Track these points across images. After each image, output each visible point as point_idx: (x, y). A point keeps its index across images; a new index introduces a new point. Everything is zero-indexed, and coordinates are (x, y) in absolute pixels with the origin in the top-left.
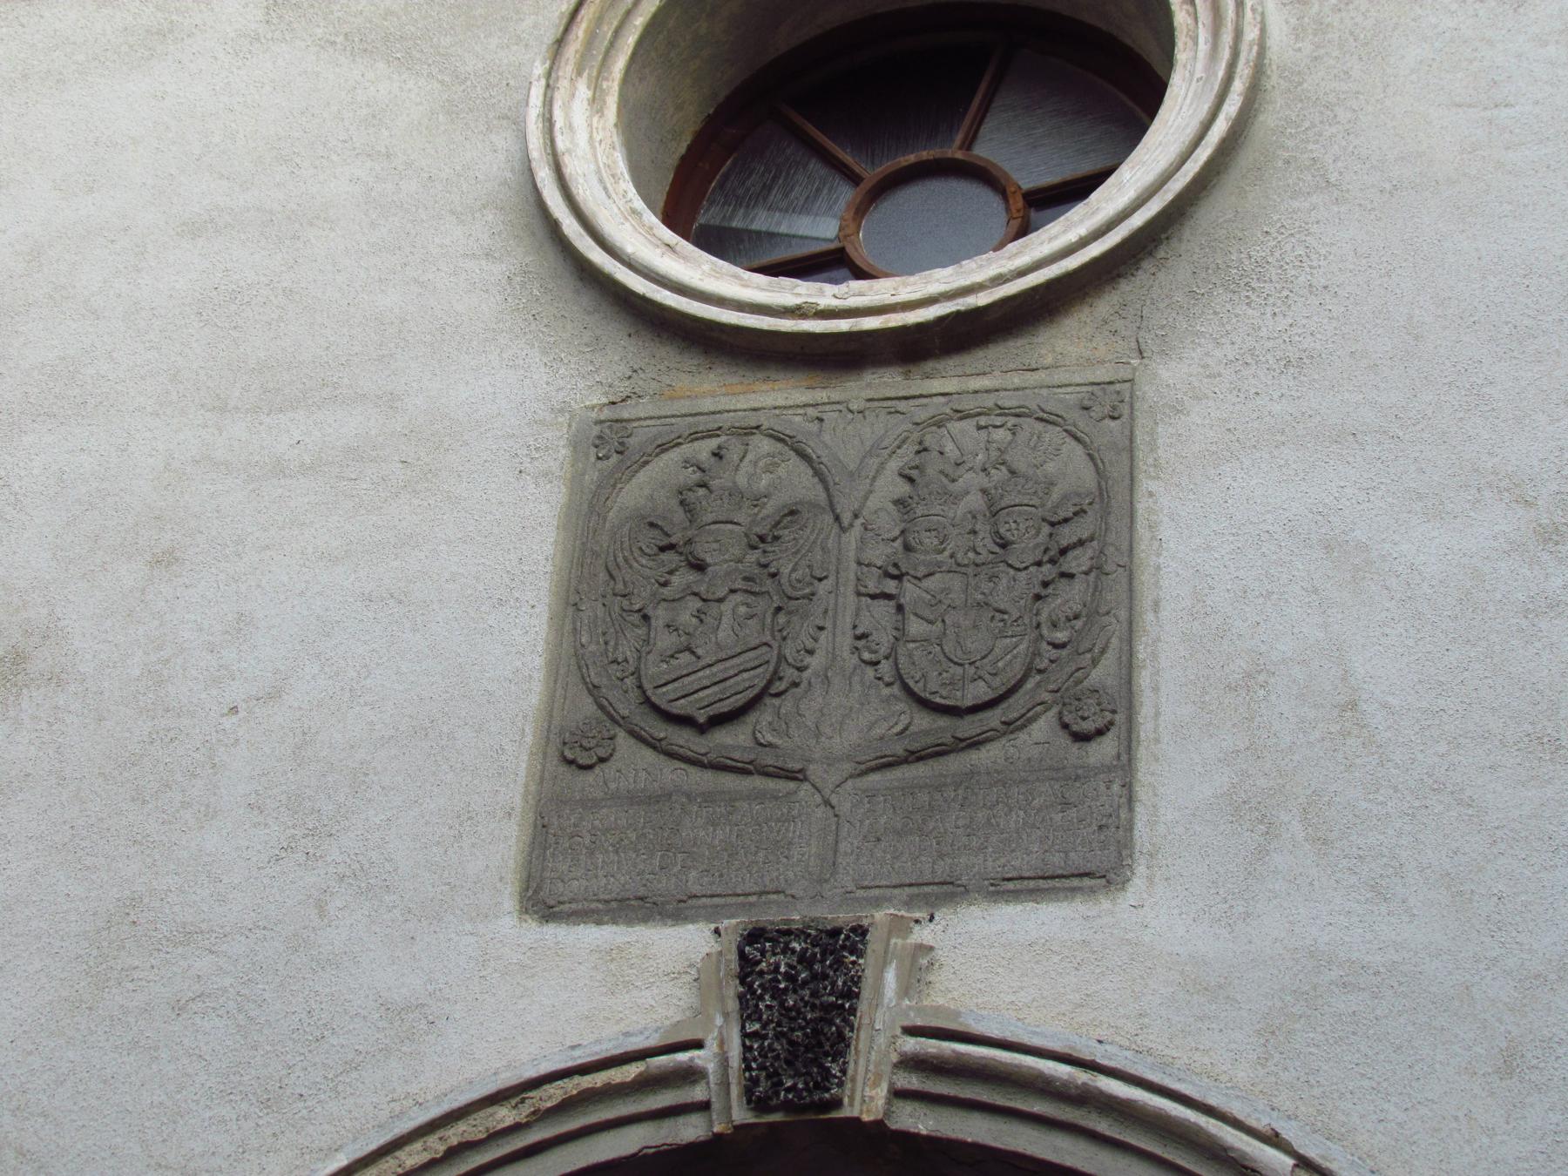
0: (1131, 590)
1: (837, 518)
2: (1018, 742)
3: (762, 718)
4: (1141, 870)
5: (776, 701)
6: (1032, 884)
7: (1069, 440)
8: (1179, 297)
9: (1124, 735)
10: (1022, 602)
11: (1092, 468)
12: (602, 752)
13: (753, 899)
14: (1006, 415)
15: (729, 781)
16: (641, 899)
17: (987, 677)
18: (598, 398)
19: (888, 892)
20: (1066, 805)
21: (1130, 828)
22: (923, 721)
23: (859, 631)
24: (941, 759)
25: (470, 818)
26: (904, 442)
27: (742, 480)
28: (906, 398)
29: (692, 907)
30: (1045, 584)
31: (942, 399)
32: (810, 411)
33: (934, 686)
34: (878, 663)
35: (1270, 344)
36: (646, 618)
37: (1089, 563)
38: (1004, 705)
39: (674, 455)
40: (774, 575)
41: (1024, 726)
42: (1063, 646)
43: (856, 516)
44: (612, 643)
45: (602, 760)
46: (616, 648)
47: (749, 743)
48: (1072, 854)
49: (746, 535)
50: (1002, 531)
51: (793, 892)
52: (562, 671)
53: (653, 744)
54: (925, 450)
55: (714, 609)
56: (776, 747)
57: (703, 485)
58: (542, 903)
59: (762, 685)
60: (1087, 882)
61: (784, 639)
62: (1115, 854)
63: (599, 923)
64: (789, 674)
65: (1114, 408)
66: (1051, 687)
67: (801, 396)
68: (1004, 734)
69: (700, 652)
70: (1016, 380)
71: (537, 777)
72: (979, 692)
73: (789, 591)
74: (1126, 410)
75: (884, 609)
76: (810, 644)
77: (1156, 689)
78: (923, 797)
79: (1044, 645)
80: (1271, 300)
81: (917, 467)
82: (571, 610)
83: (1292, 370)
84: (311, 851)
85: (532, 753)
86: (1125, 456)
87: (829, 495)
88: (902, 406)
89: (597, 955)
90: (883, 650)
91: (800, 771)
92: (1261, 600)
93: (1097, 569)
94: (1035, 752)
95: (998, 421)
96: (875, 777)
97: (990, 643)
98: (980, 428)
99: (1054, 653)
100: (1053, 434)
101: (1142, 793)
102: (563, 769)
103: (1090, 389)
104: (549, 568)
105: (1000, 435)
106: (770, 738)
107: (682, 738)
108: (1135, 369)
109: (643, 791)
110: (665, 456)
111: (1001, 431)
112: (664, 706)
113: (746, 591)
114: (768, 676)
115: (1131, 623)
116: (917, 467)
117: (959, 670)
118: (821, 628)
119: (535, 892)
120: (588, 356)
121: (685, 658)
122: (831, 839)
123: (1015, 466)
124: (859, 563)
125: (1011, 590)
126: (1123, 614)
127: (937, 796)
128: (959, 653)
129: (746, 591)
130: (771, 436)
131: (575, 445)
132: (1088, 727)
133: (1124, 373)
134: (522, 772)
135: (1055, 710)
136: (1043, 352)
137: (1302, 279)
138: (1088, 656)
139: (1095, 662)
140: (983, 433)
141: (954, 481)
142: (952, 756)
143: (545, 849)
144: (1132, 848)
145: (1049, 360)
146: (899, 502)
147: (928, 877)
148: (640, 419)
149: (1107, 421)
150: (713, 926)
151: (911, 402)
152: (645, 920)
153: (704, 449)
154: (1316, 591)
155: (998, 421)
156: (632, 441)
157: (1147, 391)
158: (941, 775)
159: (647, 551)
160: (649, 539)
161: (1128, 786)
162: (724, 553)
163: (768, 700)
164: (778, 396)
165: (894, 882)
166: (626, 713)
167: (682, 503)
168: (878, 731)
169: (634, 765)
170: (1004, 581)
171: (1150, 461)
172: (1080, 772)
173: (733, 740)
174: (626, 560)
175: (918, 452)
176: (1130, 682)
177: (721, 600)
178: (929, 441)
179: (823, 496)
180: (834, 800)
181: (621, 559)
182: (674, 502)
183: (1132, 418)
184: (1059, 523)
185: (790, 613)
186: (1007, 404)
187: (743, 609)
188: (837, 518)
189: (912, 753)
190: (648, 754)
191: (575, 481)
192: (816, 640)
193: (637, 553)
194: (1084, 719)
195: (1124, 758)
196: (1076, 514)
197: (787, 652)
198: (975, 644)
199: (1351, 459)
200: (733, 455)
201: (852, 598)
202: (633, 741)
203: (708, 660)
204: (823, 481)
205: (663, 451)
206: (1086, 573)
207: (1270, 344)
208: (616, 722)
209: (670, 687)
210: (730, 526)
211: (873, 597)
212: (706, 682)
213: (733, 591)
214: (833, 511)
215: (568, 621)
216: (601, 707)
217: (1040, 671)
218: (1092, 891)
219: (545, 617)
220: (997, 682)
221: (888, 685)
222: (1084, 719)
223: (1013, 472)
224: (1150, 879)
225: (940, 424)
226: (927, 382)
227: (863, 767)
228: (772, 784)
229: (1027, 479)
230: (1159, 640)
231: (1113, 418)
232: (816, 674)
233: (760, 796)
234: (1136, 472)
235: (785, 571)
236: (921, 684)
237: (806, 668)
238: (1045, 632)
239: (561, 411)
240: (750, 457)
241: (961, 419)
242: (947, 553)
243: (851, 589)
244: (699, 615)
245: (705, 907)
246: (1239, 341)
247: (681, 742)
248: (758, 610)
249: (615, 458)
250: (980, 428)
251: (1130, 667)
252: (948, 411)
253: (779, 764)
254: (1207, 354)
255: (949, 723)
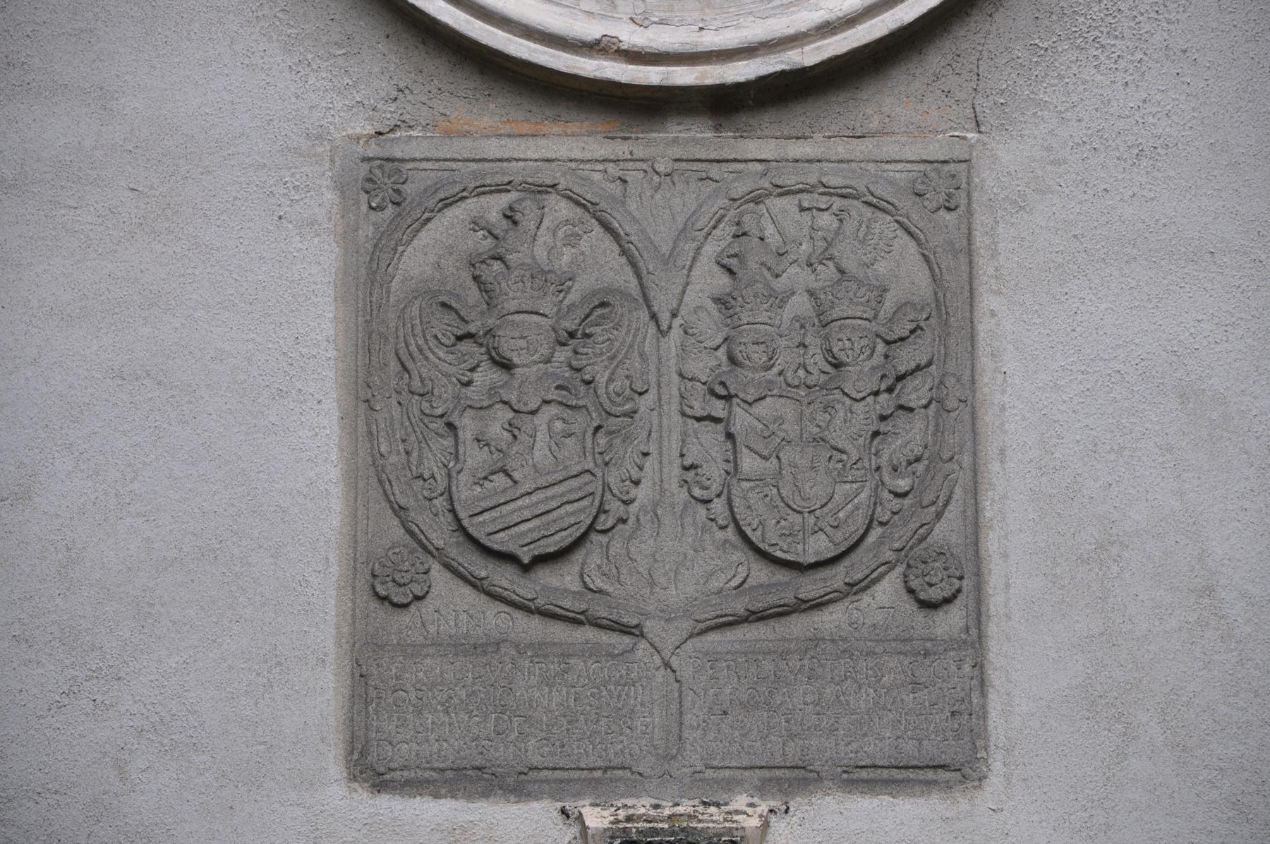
0: (974, 432)
1: (654, 317)
2: (863, 604)
3: (592, 557)
4: (997, 766)
5: (603, 539)
6: (885, 774)
7: (900, 232)
8: (1019, 51)
9: (972, 605)
10: (861, 441)
11: (927, 272)
12: (418, 590)
13: (598, 774)
14: (831, 194)
15: (559, 632)
16: (479, 769)
17: (828, 529)
18: (362, 127)
19: (738, 773)
20: (916, 685)
21: (984, 716)
22: (761, 573)
23: (688, 462)
24: (783, 620)
25: (279, 664)
26: (719, 221)
27: (541, 253)
28: (718, 161)
29: (535, 781)
30: (883, 418)
31: (759, 167)
32: (611, 167)
33: (771, 539)
34: (710, 501)
35: (1121, 125)
36: (450, 426)
37: (929, 395)
38: (846, 562)
39: (458, 212)
40: (588, 383)
41: (868, 587)
42: (905, 495)
43: (674, 315)
44: (415, 454)
45: (418, 598)
46: (420, 463)
47: (576, 586)
48: (925, 742)
49: (554, 330)
50: (835, 350)
51: (641, 769)
52: (361, 485)
53: (475, 584)
54: (744, 234)
55: (526, 423)
56: (608, 594)
57: (499, 258)
58: (372, 771)
59: (588, 522)
60: (943, 775)
61: (607, 464)
62: (970, 745)
63: (437, 796)
64: (615, 506)
65: (949, 196)
66: (897, 545)
67: (598, 148)
68: (846, 596)
69: (516, 475)
70: (840, 149)
71: (348, 617)
72: (819, 546)
73: (607, 405)
74: (963, 202)
75: (711, 436)
76: (635, 474)
77: (1005, 556)
78: (768, 665)
79: (886, 495)
80: (1122, 64)
81: (736, 256)
82: (362, 406)
83: (1144, 162)
84: (99, 697)
85: (340, 588)
86: (963, 259)
87: (642, 285)
88: (714, 171)
89: (438, 835)
90: (715, 488)
91: (636, 626)
92: (1113, 456)
93: (936, 401)
94: (879, 617)
95: (823, 202)
96: (714, 637)
97: (830, 490)
98: (802, 209)
99: (896, 504)
100: (884, 225)
101: (994, 677)
102: (374, 604)
103: (922, 167)
104: (332, 353)
105: (825, 220)
106: (599, 583)
107: (503, 577)
108: (971, 146)
109: (467, 636)
110: (450, 212)
111: (826, 215)
112: (484, 540)
113: (561, 403)
114: (594, 511)
115: (975, 472)
116: (736, 256)
117: (797, 519)
118: (646, 454)
119: (362, 754)
120: (341, 61)
121: (500, 480)
122: (674, 707)
123: (844, 264)
124: (681, 375)
125: (849, 424)
126: (966, 459)
127: (782, 665)
128: (797, 498)
129: (561, 403)
130: (569, 198)
131: (341, 188)
132: (935, 594)
133: (959, 152)
134: (332, 611)
135: (900, 569)
136: (869, 111)
137: (1157, 37)
138: (933, 509)
139: (939, 516)
140: (806, 217)
141: (777, 276)
142: (794, 616)
143: (367, 704)
144: (987, 739)
145: (874, 125)
146: (722, 302)
147: (779, 761)
148: (414, 160)
149: (942, 212)
150: (559, 805)
151: (724, 166)
152: (486, 794)
153: (494, 206)
154: (1170, 449)
155: (823, 202)
156: (407, 189)
157: (987, 179)
158: (784, 639)
159: (443, 340)
160: (444, 325)
161: (979, 666)
162: (526, 341)
163: (595, 537)
164: (571, 144)
165: (745, 764)
166: (441, 544)
167: (476, 278)
168: (716, 584)
169: (451, 605)
170: (841, 414)
171: (991, 270)
172: (928, 645)
173: (561, 582)
174: (421, 351)
175: (736, 236)
176: (976, 543)
177: (533, 413)
178: (749, 223)
179: (634, 282)
180: (675, 662)
181: (413, 348)
182: (466, 275)
183: (970, 213)
184: (895, 342)
185: (611, 433)
186: (833, 181)
187: (558, 425)
188: (654, 317)
189: (754, 613)
190: (467, 590)
191: (347, 237)
192: (641, 469)
193: (432, 343)
194: (931, 585)
195: (973, 631)
196: (912, 332)
197: (611, 480)
198: (815, 488)
199: (1209, 286)
200: (528, 220)
201: (677, 418)
202: (449, 575)
203: (527, 487)
204: (633, 264)
205: (446, 206)
206: (926, 407)
207: (1121, 125)
208: (429, 552)
209: (487, 516)
210: (535, 318)
211: (699, 419)
212: (527, 514)
213: (546, 402)
214: (649, 307)
215: (360, 423)
216: (410, 532)
217: (882, 524)
218: (948, 786)
219: (336, 414)
220: (839, 536)
221: (723, 528)
222: (931, 585)
223: (842, 271)
224: (1008, 778)
225: (757, 201)
226: (742, 143)
227: (702, 626)
228: (605, 638)
229: (860, 283)
230: (1005, 497)
231: (949, 209)
232: (643, 508)
233: (594, 652)
234: (976, 283)
235: (602, 380)
236: (759, 533)
237: (632, 501)
238: (886, 478)
239: (319, 137)
240: (546, 222)
241: (780, 195)
242: (775, 370)
243: (675, 407)
244: (511, 427)
245: (547, 781)
246: (1086, 118)
247: (505, 584)
248: (576, 428)
249: (390, 210)
250: (802, 209)
251: (976, 525)
252: (767, 185)
253: (614, 617)
254: (1051, 132)
255: (791, 581)
